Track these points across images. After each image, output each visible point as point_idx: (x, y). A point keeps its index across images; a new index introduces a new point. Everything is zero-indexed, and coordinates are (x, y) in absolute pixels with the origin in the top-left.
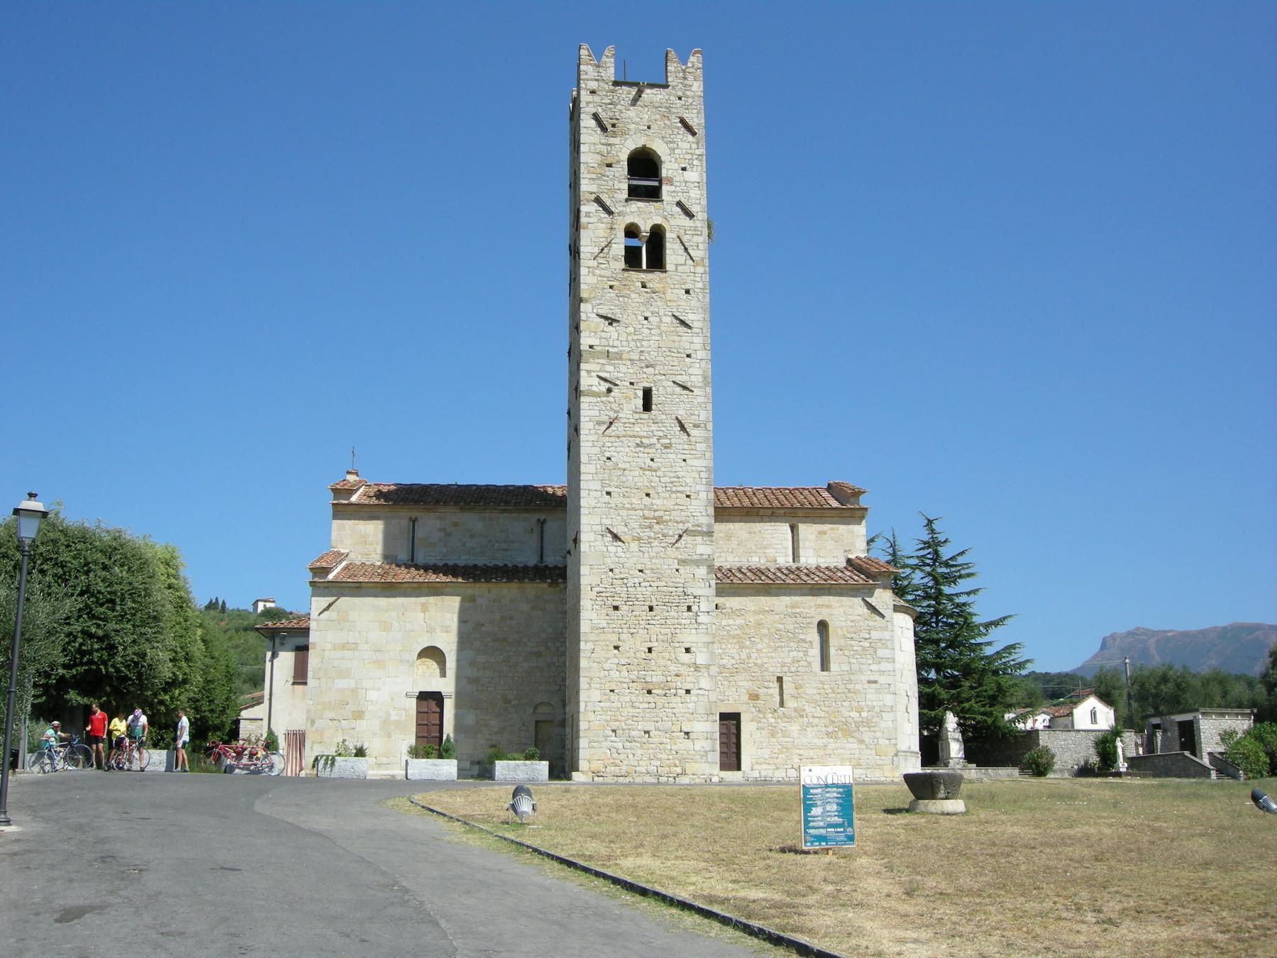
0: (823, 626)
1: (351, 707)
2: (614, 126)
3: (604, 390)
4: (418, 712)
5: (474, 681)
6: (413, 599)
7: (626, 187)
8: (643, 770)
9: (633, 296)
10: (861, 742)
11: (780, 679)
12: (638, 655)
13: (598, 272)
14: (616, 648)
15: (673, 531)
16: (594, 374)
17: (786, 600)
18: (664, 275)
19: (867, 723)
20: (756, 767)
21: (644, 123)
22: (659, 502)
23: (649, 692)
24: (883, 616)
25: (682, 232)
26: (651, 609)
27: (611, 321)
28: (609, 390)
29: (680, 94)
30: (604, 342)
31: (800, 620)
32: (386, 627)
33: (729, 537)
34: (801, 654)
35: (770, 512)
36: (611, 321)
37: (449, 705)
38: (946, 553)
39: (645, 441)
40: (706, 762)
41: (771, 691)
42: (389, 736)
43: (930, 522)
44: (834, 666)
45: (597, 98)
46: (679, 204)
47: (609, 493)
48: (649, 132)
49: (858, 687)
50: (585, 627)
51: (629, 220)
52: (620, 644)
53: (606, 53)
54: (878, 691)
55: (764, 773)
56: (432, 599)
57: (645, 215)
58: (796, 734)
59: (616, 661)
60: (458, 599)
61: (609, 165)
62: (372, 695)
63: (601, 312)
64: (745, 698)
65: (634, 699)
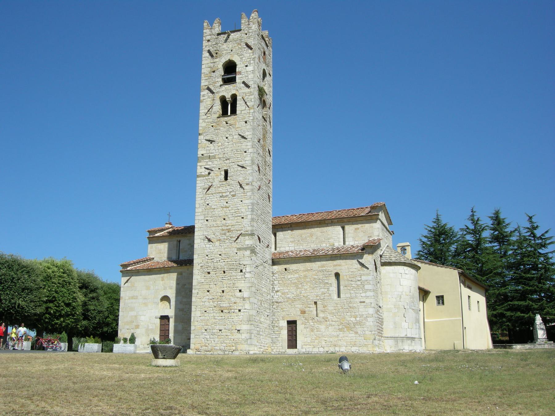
0: (337, 275)
1: (135, 324)
2: (217, 53)
3: (207, 173)
4: (161, 325)
7: (221, 79)
8: (218, 348)
9: (221, 128)
10: (356, 333)
11: (316, 303)
12: (217, 294)
13: (207, 121)
14: (208, 291)
15: (235, 235)
17: (318, 264)
18: (236, 116)
19: (360, 323)
20: (304, 347)
21: (230, 50)
22: (229, 222)
23: (222, 311)
24: (368, 269)
25: (244, 95)
26: (224, 272)
27: (211, 141)
28: (209, 173)
29: (246, 32)
30: (208, 152)
31: (325, 273)
32: (148, 288)
33: (312, 235)
34: (326, 290)
35: (330, 221)
36: (211, 141)
37: (172, 321)
38: (538, 233)
39: (223, 194)
40: (247, 344)
41: (311, 309)
43: (531, 218)
44: (342, 295)
45: (210, 43)
46: (244, 83)
47: (207, 220)
48: (232, 53)
49: (354, 305)
50: (195, 283)
51: (221, 94)
52: (210, 289)
53: (215, 22)
54: (365, 307)
55: (308, 350)
56: (166, 275)
57: (227, 91)
58: (323, 330)
59: (208, 297)
60: (176, 274)
61: (214, 72)
62: (143, 318)
63: (207, 138)
64: (299, 313)
65: (215, 315)
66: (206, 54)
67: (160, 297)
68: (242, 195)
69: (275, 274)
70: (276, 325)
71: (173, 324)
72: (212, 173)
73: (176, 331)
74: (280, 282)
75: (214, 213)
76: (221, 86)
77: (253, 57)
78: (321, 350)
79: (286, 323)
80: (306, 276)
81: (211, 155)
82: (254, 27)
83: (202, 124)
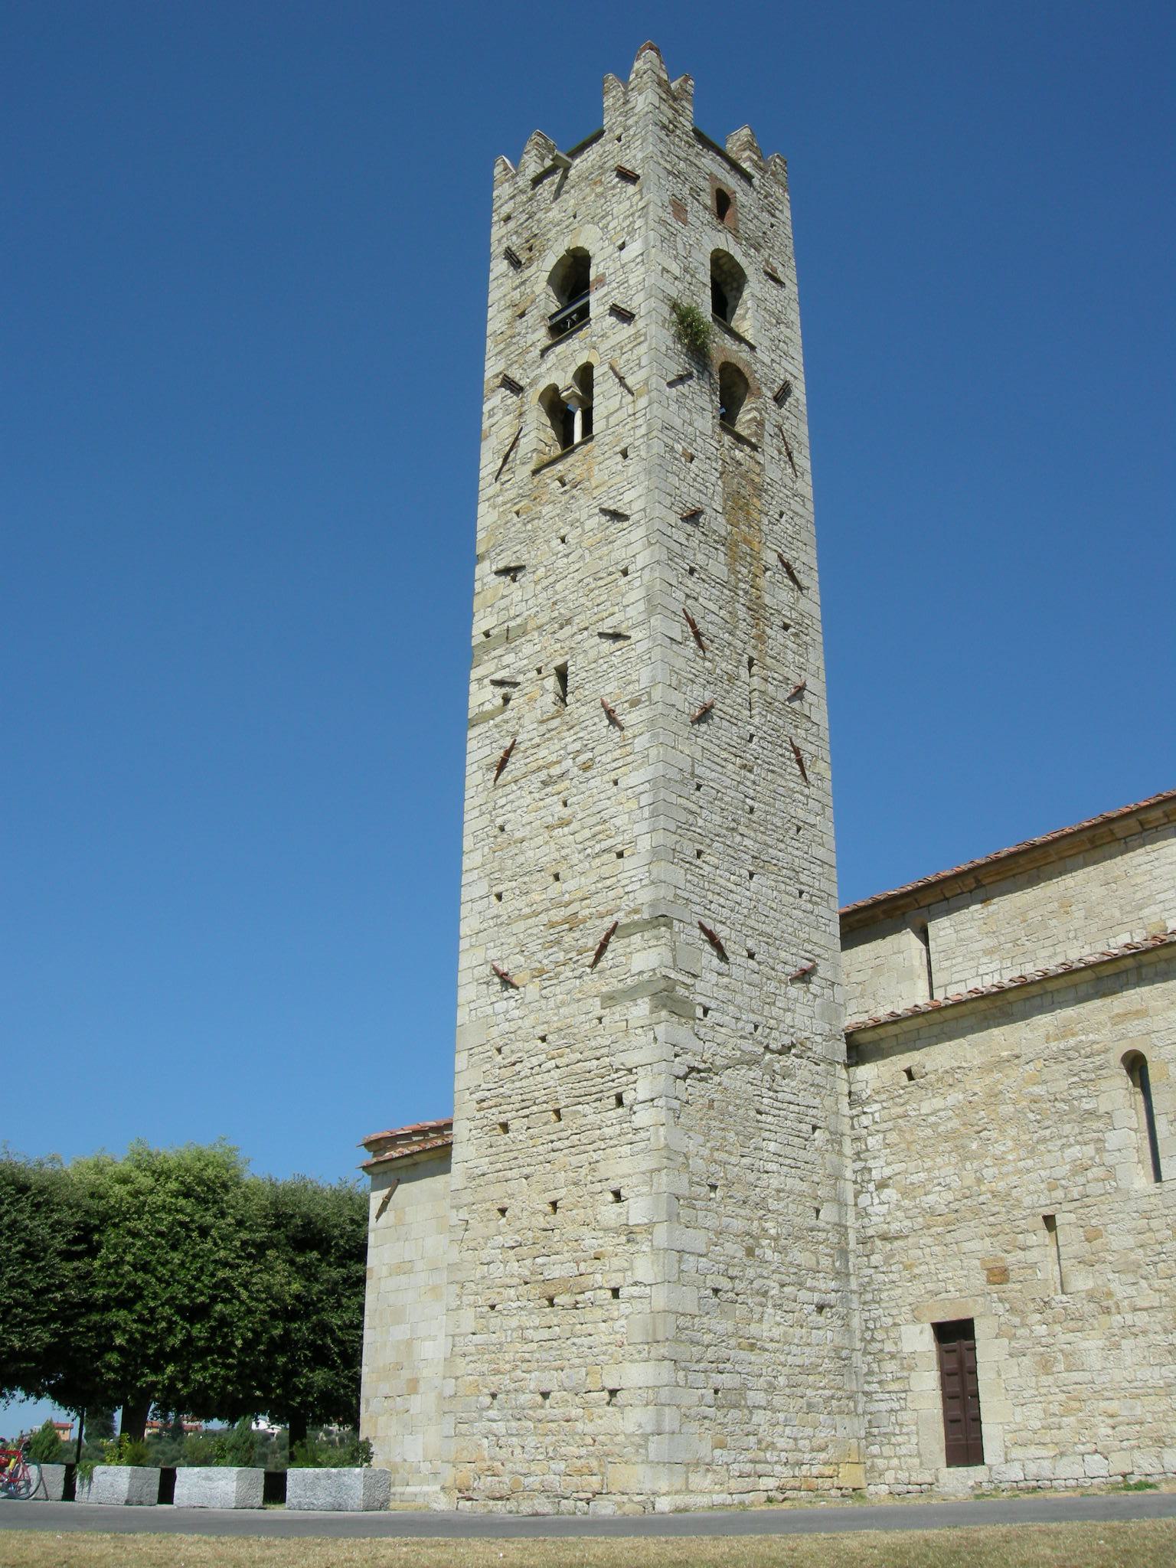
0: (1136, 1065)
1: (406, 1374)
8: (533, 1481)
9: (545, 510)
11: (1049, 1221)
16: (487, 681)
17: (1044, 1021)
20: (1017, 1453)
28: (506, 700)
30: (504, 615)
33: (1066, 906)
34: (1090, 1150)
35: (1132, 822)
40: (646, 1462)
41: (1033, 1256)
45: (512, 224)
52: (506, 1202)
55: (1032, 1468)
58: (1094, 1361)
61: (522, 315)
63: (501, 565)
64: (980, 1280)
66: (499, 266)
68: (617, 754)
69: (864, 1103)
70: (889, 1347)
72: (515, 693)
74: (892, 1138)
75: (521, 859)
76: (544, 352)
77: (641, 204)
78: (1096, 1465)
79: (929, 1335)
80: (994, 1096)
81: (512, 624)
82: (645, 100)
83: (486, 516)
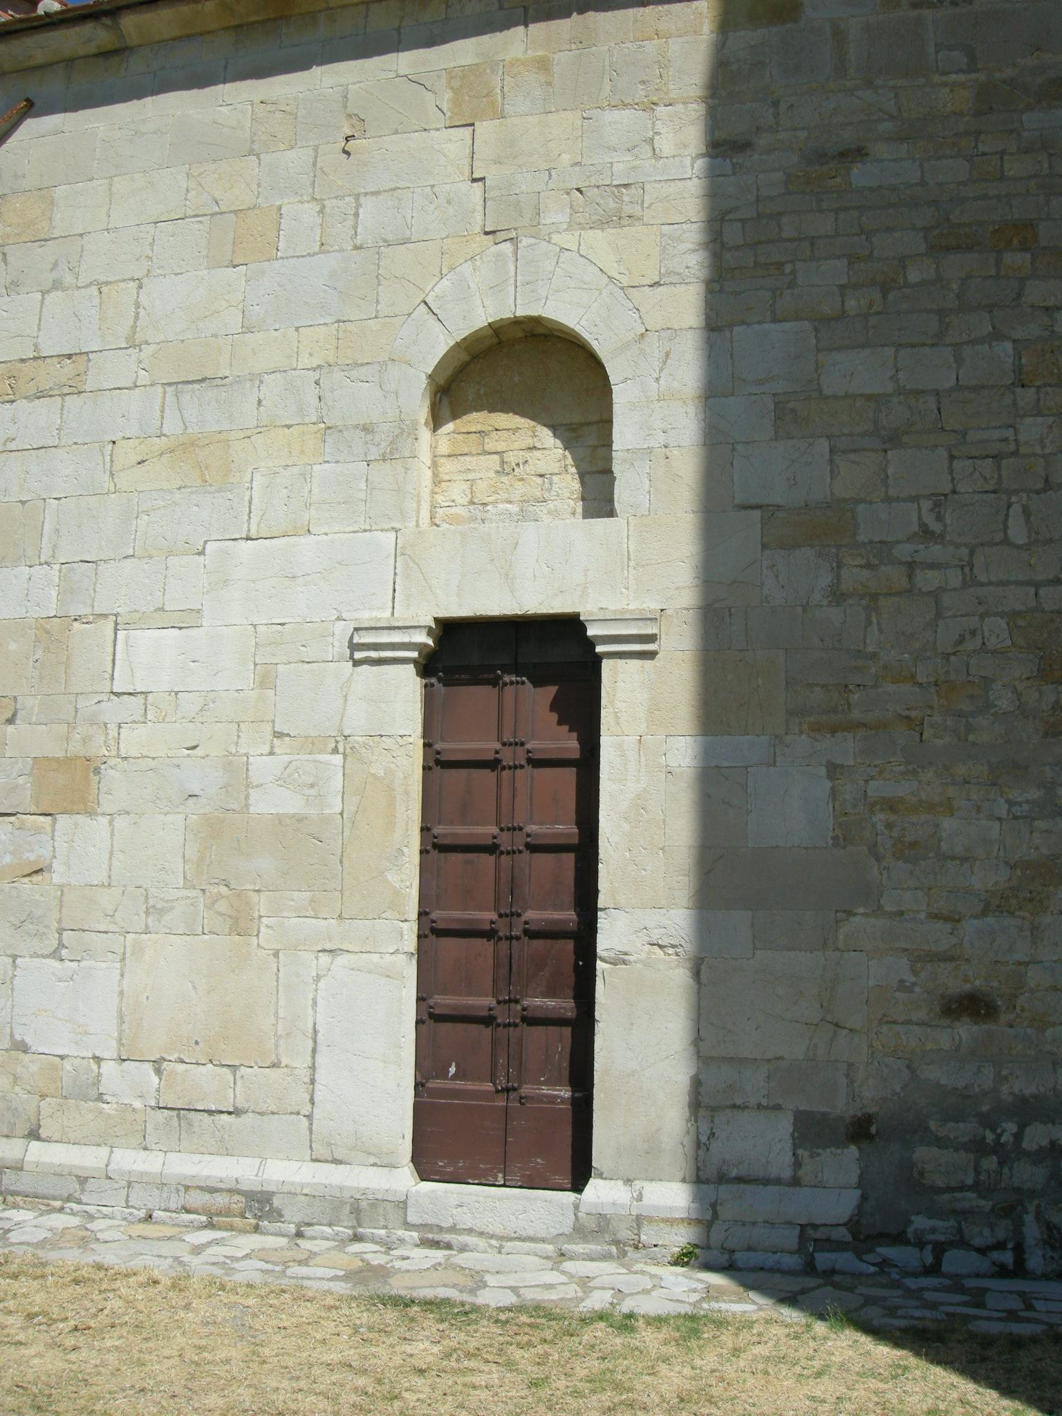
4: (437, 763)
5: (816, 527)
6: (405, 61)
32: (241, 238)
42: (241, 923)
56: (516, 43)
62: (150, 657)
67: (435, 344)
71: (682, 752)
73: (729, 875)
